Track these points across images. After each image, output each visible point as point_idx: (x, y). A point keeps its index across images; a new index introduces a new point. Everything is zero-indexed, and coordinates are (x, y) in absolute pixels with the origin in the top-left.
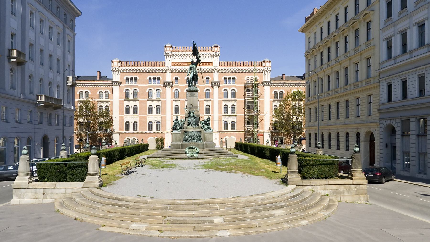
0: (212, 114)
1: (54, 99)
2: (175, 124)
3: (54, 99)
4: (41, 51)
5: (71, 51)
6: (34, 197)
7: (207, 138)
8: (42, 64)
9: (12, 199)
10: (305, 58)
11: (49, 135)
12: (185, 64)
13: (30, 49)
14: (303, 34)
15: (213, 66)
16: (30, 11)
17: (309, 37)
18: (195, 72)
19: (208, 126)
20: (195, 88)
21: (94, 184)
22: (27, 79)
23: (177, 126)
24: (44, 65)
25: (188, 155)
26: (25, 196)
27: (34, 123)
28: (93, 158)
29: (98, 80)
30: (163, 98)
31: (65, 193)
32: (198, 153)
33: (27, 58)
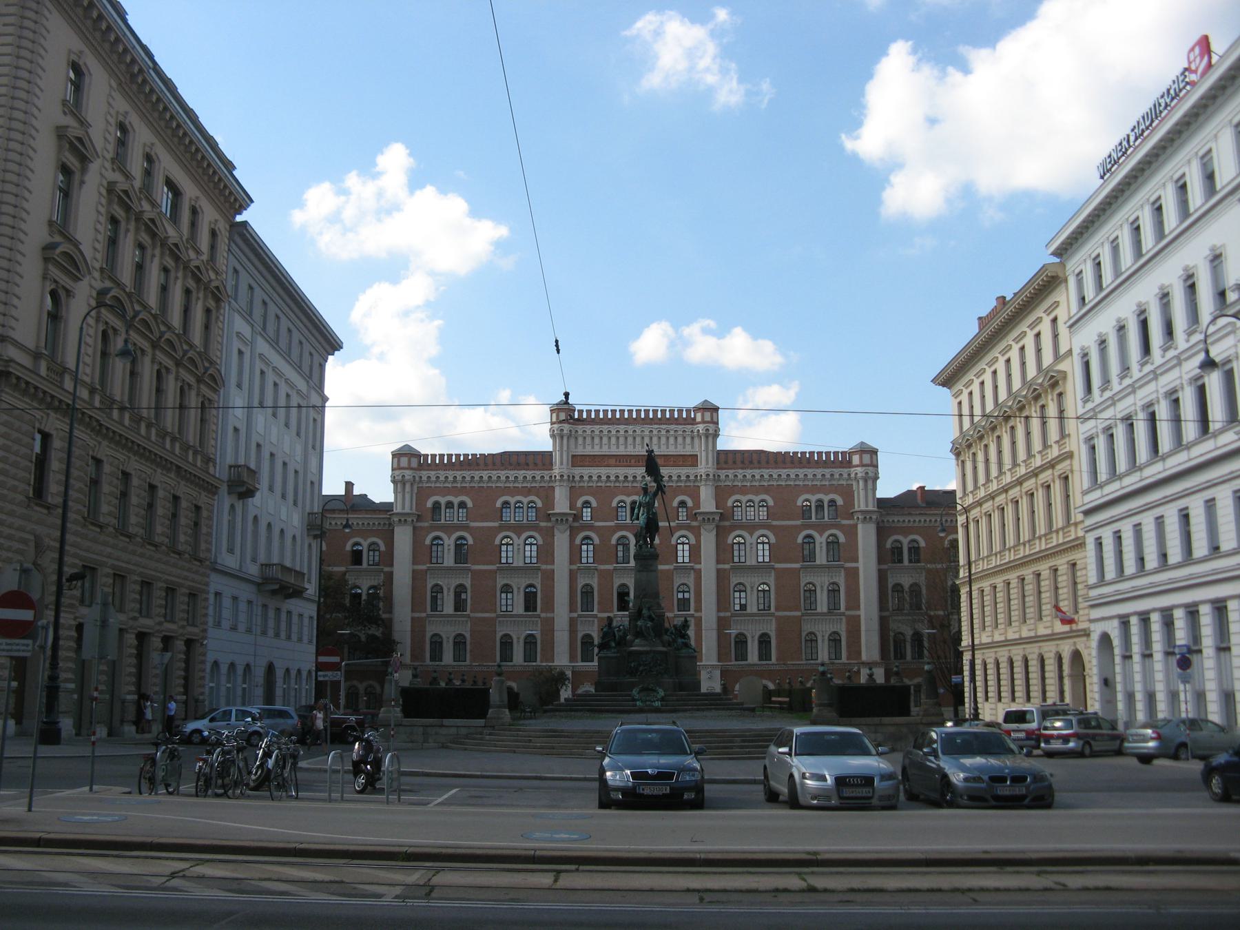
0: (696, 611)
17: (958, 400)
32: (662, 699)
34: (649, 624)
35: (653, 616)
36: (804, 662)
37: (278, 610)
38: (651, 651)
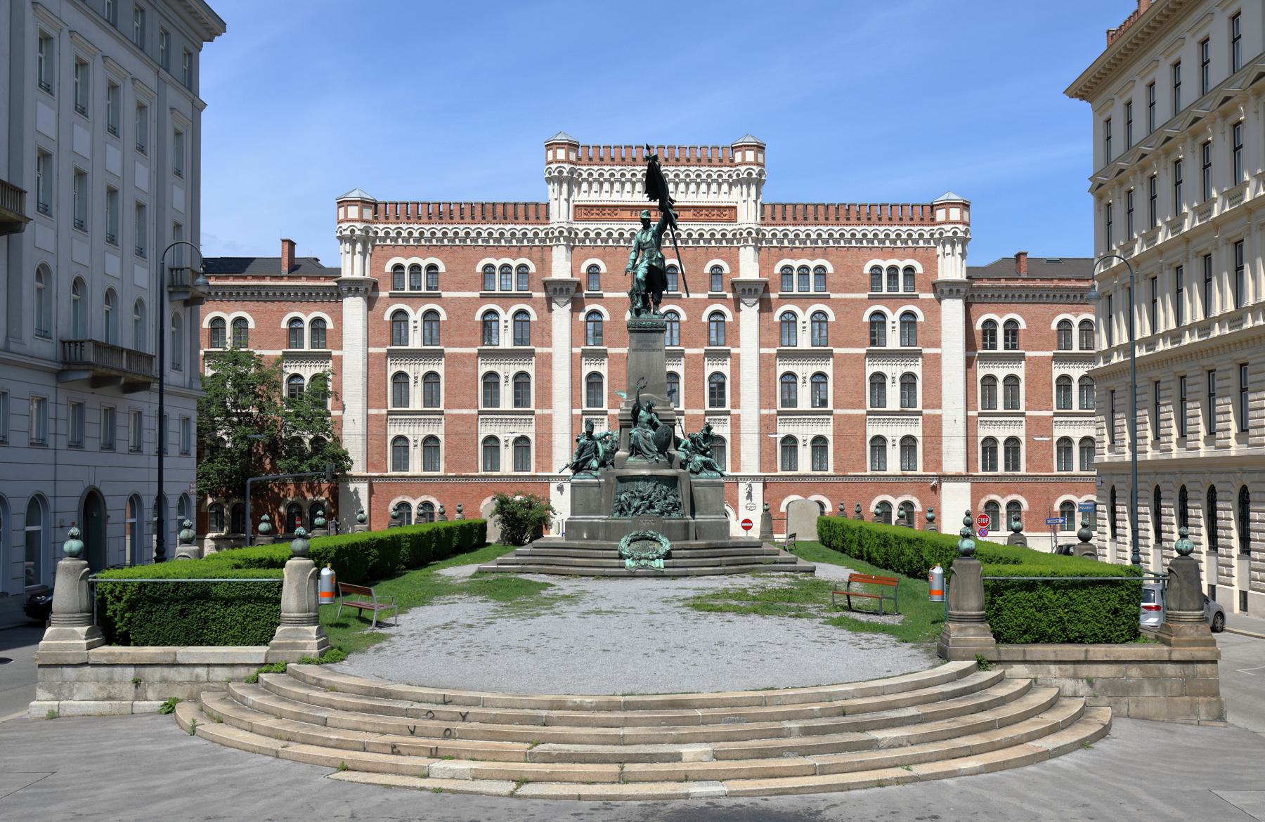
1: (124, 354)
2: (582, 449)
3: (124, 354)
4: (80, 175)
5: (187, 171)
6: (105, 694)
7: (703, 503)
8: (80, 225)
9: (34, 699)
10: (1091, 199)
11: (105, 490)
12: (627, 214)
13: (38, 170)
14: (1086, 106)
15: (739, 221)
16: (41, 32)
17: (1105, 117)
18: (655, 261)
19: (706, 456)
20: (656, 317)
21: (303, 651)
22: (29, 284)
23: (589, 459)
24: (89, 229)
25: (628, 562)
26: (75, 691)
27: (51, 445)
28: (300, 566)
29: (283, 274)
30: (542, 345)
31: (209, 682)
32: (668, 556)
33: (30, 208)
34: (650, 433)
35: (656, 420)
36: (869, 473)
37: (110, 413)
38: (651, 476)
